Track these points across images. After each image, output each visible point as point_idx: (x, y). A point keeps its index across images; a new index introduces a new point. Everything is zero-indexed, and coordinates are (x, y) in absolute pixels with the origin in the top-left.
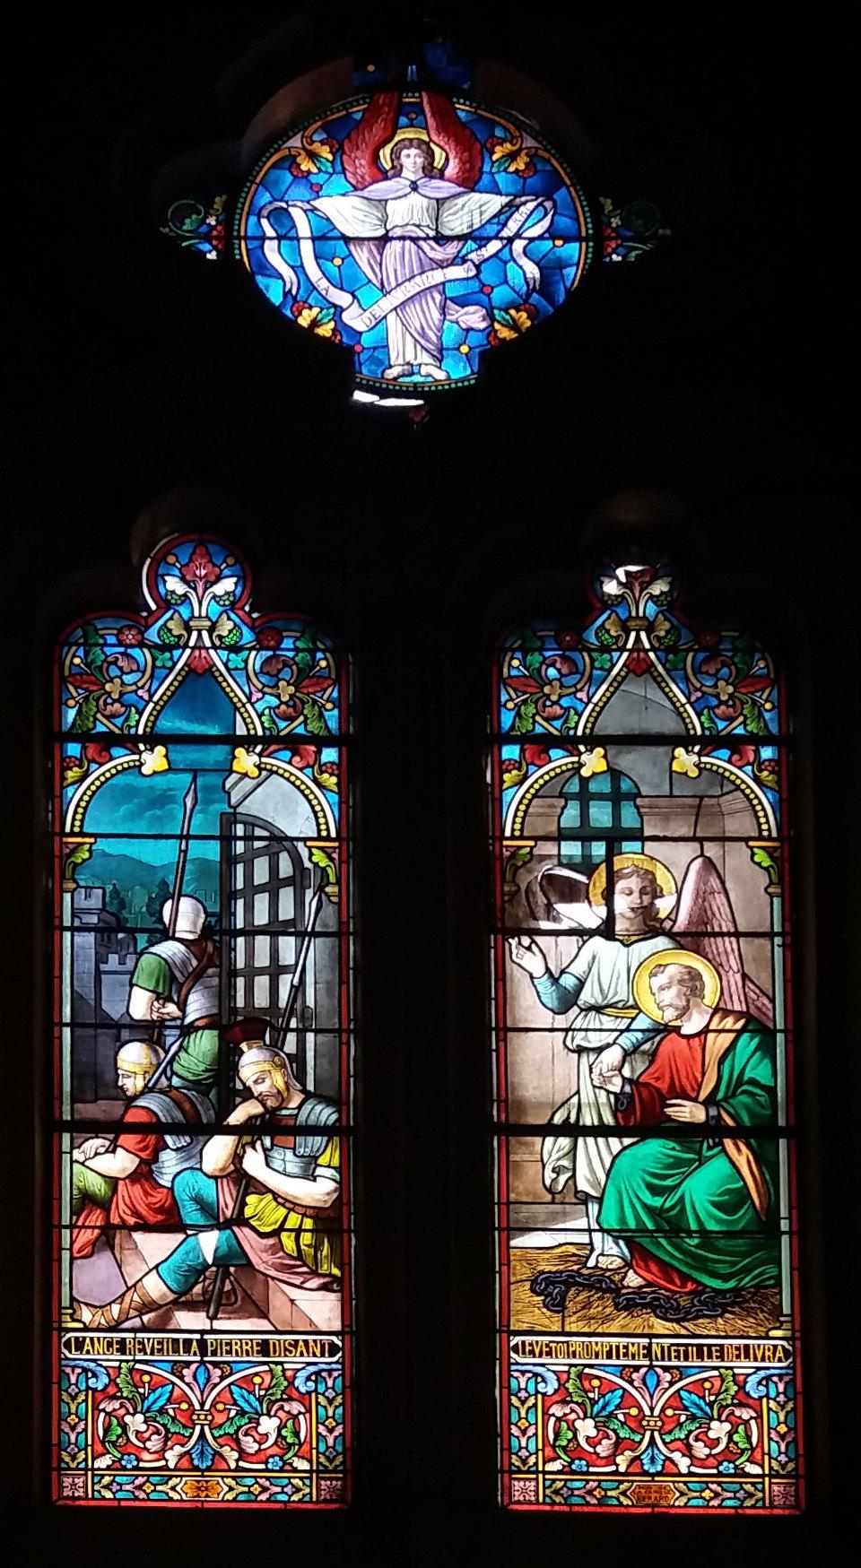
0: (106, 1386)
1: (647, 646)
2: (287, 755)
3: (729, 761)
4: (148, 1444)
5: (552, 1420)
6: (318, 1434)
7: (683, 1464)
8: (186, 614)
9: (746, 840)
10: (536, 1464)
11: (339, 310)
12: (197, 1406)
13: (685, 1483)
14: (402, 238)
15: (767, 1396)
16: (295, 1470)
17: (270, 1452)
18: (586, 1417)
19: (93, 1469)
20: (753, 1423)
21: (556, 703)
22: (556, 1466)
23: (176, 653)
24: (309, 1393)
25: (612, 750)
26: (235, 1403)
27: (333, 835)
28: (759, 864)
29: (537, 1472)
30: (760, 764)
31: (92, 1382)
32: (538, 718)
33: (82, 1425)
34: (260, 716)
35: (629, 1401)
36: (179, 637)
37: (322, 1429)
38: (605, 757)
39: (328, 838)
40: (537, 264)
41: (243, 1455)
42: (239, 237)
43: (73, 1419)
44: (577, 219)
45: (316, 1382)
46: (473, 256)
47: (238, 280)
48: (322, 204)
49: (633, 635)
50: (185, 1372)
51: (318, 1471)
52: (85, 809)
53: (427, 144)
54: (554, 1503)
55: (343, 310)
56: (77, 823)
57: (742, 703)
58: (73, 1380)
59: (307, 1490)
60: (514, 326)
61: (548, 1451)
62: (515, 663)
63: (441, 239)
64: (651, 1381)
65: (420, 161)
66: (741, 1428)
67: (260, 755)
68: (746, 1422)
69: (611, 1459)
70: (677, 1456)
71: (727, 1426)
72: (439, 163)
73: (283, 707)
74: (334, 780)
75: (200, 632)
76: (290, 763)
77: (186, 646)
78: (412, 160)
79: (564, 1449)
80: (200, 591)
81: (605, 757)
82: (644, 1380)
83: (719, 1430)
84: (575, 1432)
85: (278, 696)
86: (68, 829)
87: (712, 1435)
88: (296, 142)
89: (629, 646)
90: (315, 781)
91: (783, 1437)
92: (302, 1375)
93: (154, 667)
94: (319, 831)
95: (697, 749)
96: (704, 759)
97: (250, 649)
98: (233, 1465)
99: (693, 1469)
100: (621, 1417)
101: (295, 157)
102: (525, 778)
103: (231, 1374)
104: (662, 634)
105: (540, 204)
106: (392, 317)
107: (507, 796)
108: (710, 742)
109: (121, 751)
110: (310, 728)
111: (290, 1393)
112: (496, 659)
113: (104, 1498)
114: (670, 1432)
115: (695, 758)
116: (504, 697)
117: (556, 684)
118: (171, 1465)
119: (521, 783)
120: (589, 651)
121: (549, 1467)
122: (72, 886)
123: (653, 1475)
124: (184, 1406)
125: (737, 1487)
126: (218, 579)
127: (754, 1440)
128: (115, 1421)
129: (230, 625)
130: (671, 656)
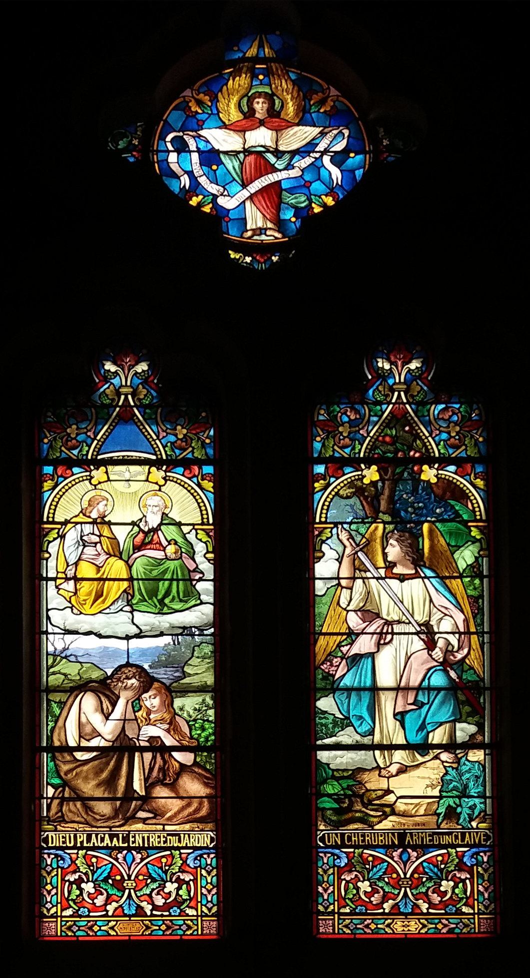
5: (344, 882)
6: (202, 893)
7: (424, 907)
8: (391, 382)
10: (56, 912)
12: (402, 876)
13: (150, 921)
15: (200, 866)
16: (187, 915)
18: (88, 881)
21: (75, 438)
22: (69, 912)
23: (384, 407)
28: (200, 540)
29: (57, 917)
32: (336, 447)
33: (54, 891)
34: (164, 447)
36: (113, 400)
37: (204, 891)
39: (208, 524)
41: (431, 905)
45: (200, 861)
47: (151, 179)
49: (396, 394)
51: (202, 916)
57: (465, 437)
59: (196, 928)
60: (324, 205)
61: (64, 901)
62: (322, 412)
64: (129, 858)
65: (266, 106)
66: (461, 885)
69: (380, 905)
71: (176, 885)
73: (179, 442)
75: (126, 395)
76: (183, 475)
77: (117, 405)
78: (260, 105)
80: (400, 369)
82: (125, 858)
85: (176, 435)
86: (45, 520)
87: (442, 889)
88: (188, 93)
89: (394, 401)
90: (199, 485)
94: (203, 519)
95: (436, 466)
96: (440, 472)
97: (431, 404)
98: (149, 913)
99: (431, 911)
101: (188, 103)
102: (329, 485)
103: (148, 857)
104: (142, 397)
105: (341, 132)
108: (444, 461)
109: (348, 470)
110: (196, 455)
112: (311, 412)
114: (416, 888)
115: (435, 472)
118: (110, 914)
120: (367, 404)
121: (64, 914)
122: (47, 555)
123: (130, 916)
124: (118, 878)
125: (182, 922)
127: (468, 894)
130: (148, 411)
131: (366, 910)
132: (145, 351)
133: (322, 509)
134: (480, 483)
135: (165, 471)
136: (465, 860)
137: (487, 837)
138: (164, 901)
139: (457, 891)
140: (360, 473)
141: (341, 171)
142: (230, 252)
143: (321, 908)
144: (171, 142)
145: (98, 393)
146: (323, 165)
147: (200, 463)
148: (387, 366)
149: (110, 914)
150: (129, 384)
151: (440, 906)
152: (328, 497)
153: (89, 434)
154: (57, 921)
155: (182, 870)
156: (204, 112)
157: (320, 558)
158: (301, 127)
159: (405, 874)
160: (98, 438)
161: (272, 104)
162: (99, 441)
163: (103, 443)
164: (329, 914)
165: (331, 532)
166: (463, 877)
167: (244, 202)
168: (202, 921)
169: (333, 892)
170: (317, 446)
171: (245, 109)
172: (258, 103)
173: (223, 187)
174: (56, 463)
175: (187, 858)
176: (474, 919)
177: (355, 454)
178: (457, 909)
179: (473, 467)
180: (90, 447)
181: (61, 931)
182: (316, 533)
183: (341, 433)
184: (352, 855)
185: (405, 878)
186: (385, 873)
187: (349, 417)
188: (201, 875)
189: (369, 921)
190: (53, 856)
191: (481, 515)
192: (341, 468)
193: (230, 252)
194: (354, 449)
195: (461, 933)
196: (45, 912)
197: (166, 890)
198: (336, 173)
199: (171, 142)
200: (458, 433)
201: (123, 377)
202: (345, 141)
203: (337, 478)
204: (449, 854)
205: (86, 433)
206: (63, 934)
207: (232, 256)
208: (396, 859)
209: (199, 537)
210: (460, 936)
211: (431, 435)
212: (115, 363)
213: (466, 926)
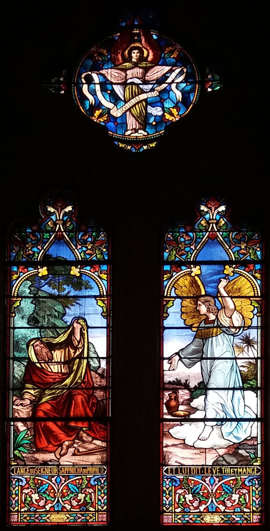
4: (194, 504)
5: (178, 495)
7: (68, 507)
9: (249, 297)
11: (109, 110)
12: (211, 492)
15: (97, 484)
17: (236, 506)
18: (35, 493)
19: (175, 512)
20: (247, 494)
21: (184, 250)
22: (26, 509)
24: (249, 486)
27: (259, 295)
29: (172, 513)
31: (20, 483)
34: (234, 254)
36: (52, 228)
37: (254, 498)
38: (200, 269)
41: (72, 507)
46: (156, 89)
50: (53, 479)
55: (110, 109)
56: (169, 293)
57: (249, 249)
58: (14, 483)
61: (176, 505)
65: (138, 54)
67: (234, 268)
69: (44, 507)
70: (66, 505)
72: (145, 55)
74: (106, 276)
76: (90, 271)
78: (136, 54)
81: (200, 269)
82: (56, 480)
83: (235, 497)
84: (31, 498)
86: (165, 295)
87: (233, 499)
88: (94, 49)
89: (209, 230)
90: (99, 276)
92: (93, 479)
93: (196, 237)
94: (255, 294)
95: (79, 266)
99: (72, 510)
100: (201, 494)
102: (172, 276)
107: (165, 283)
109: (183, 268)
110: (252, 257)
113: (178, 523)
115: (78, 270)
119: (170, 278)
128: (28, 496)
129: (223, 222)
135: (80, 269)
136: (246, 483)
138: (77, 503)
140: (190, 270)
146: (172, 90)
148: (206, 210)
151: (231, 508)
152: (171, 283)
153: (191, 247)
154: (18, 515)
155: (87, 487)
157: (167, 317)
158: (164, 67)
159: (212, 491)
160: (198, 248)
162: (228, 250)
163: (226, 251)
166: (90, 492)
168: (98, 514)
170: (166, 255)
172: (134, 53)
175: (245, 481)
177: (188, 259)
180: (192, 254)
181: (21, 520)
182: (165, 303)
183: (27, 248)
184: (29, 479)
185: (58, 492)
186: (201, 490)
187: (184, 239)
190: (16, 480)
192: (180, 267)
194: (188, 255)
196: (12, 509)
197: (79, 498)
203: (177, 273)
205: (190, 247)
206: (176, 522)
208: (207, 482)
209: (172, 304)
210: (243, 525)
211: (230, 248)
212: (54, 207)
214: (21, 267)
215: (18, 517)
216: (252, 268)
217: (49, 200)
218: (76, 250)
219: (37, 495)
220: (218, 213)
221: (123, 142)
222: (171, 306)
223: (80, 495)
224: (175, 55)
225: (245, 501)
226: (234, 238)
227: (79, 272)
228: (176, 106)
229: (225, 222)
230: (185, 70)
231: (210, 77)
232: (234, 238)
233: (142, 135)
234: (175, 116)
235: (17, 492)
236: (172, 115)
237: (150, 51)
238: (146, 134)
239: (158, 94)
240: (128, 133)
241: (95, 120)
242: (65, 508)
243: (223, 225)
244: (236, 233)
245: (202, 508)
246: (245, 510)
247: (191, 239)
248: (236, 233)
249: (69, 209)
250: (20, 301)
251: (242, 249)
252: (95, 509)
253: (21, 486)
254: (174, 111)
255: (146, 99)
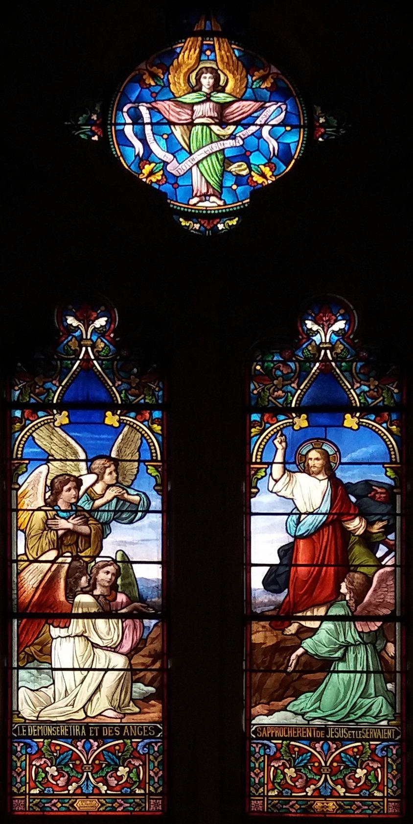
0: (275, 753)
1: (330, 358)
2: (373, 417)
3: (374, 421)
6: (150, 775)
7: (104, 789)
9: (383, 464)
10: (263, 792)
11: (166, 164)
12: (323, 764)
14: (202, 124)
15: (387, 756)
18: (291, 767)
21: (42, 386)
22: (37, 791)
24: (144, 754)
25: (313, 416)
26: (105, 760)
30: (152, 420)
33: (24, 773)
35: (338, 758)
36: (314, 355)
37: (152, 773)
38: (68, 416)
39: (156, 461)
40: (276, 140)
42: (111, 124)
43: (19, 770)
44: (299, 115)
45: (148, 748)
48: (160, 105)
49: (84, 349)
51: (388, 797)
52: (263, 449)
53: (216, 70)
54: (34, 811)
55: (168, 163)
57: (382, 390)
63: (223, 124)
65: (212, 81)
68: (137, 767)
72: (222, 83)
74: (159, 428)
79: (279, 784)
82: (83, 747)
83: (122, 771)
88: (143, 66)
90: (150, 429)
91: (394, 777)
95: (358, 415)
99: (347, 794)
105: (280, 107)
106: (195, 169)
109: (281, 417)
111: (135, 755)
114: (97, 773)
116: (252, 387)
117: (280, 379)
121: (32, 792)
124: (316, 764)
126: (336, 321)
129: (102, 345)
131: (53, 791)
132: (342, 311)
133: (258, 451)
134: (157, 428)
137: (397, 733)
138: (116, 782)
139: (131, 775)
141: (278, 143)
142: (181, 220)
143: (15, 790)
144: (127, 112)
145: (62, 346)
147: (152, 408)
149: (309, 794)
150: (89, 337)
154: (263, 800)
156: (157, 85)
160: (302, 387)
161: (217, 79)
162: (349, 390)
164: (22, 794)
165: (265, 472)
167: (191, 168)
169: (264, 776)
171: (193, 81)
173: (173, 154)
174: (262, 411)
176: (383, 802)
177: (287, 404)
178: (131, 791)
179: (389, 415)
182: (253, 472)
184: (280, 746)
185: (88, 764)
186: (70, 759)
187: (282, 371)
188: (149, 760)
189: (55, 801)
191: (396, 458)
193: (181, 220)
195: (134, 811)
198: (273, 144)
199: (127, 112)
200: (376, 387)
201: (90, 332)
202: (284, 114)
204: (125, 744)
207: (183, 224)
209: (388, 474)
211: (352, 388)
212: (77, 319)
213: (377, 807)
214: (27, 412)
215: (264, 803)
216: (148, 415)
217: (70, 307)
218: (352, 391)
219: (293, 770)
220: (95, 330)
221: (188, 216)
222: (262, 477)
223: (121, 768)
224: (267, 84)
225: (373, 780)
226: (360, 373)
227: (119, 421)
228: (269, 163)
229: (345, 347)
230: (284, 107)
231: (322, 120)
232: (360, 373)
233: (215, 205)
234: (268, 176)
235: (262, 764)
236: (263, 175)
237: (230, 76)
238: (221, 203)
239: (241, 142)
240: (194, 201)
241: (144, 180)
242: (98, 789)
243: (103, 348)
244: (361, 364)
245: (309, 791)
246: (377, 794)
247: (292, 372)
248: (361, 364)
249: (340, 325)
250: (27, 464)
251: (132, 387)
252: (145, 790)
253: (30, 754)
254: (267, 171)
255: (223, 150)
